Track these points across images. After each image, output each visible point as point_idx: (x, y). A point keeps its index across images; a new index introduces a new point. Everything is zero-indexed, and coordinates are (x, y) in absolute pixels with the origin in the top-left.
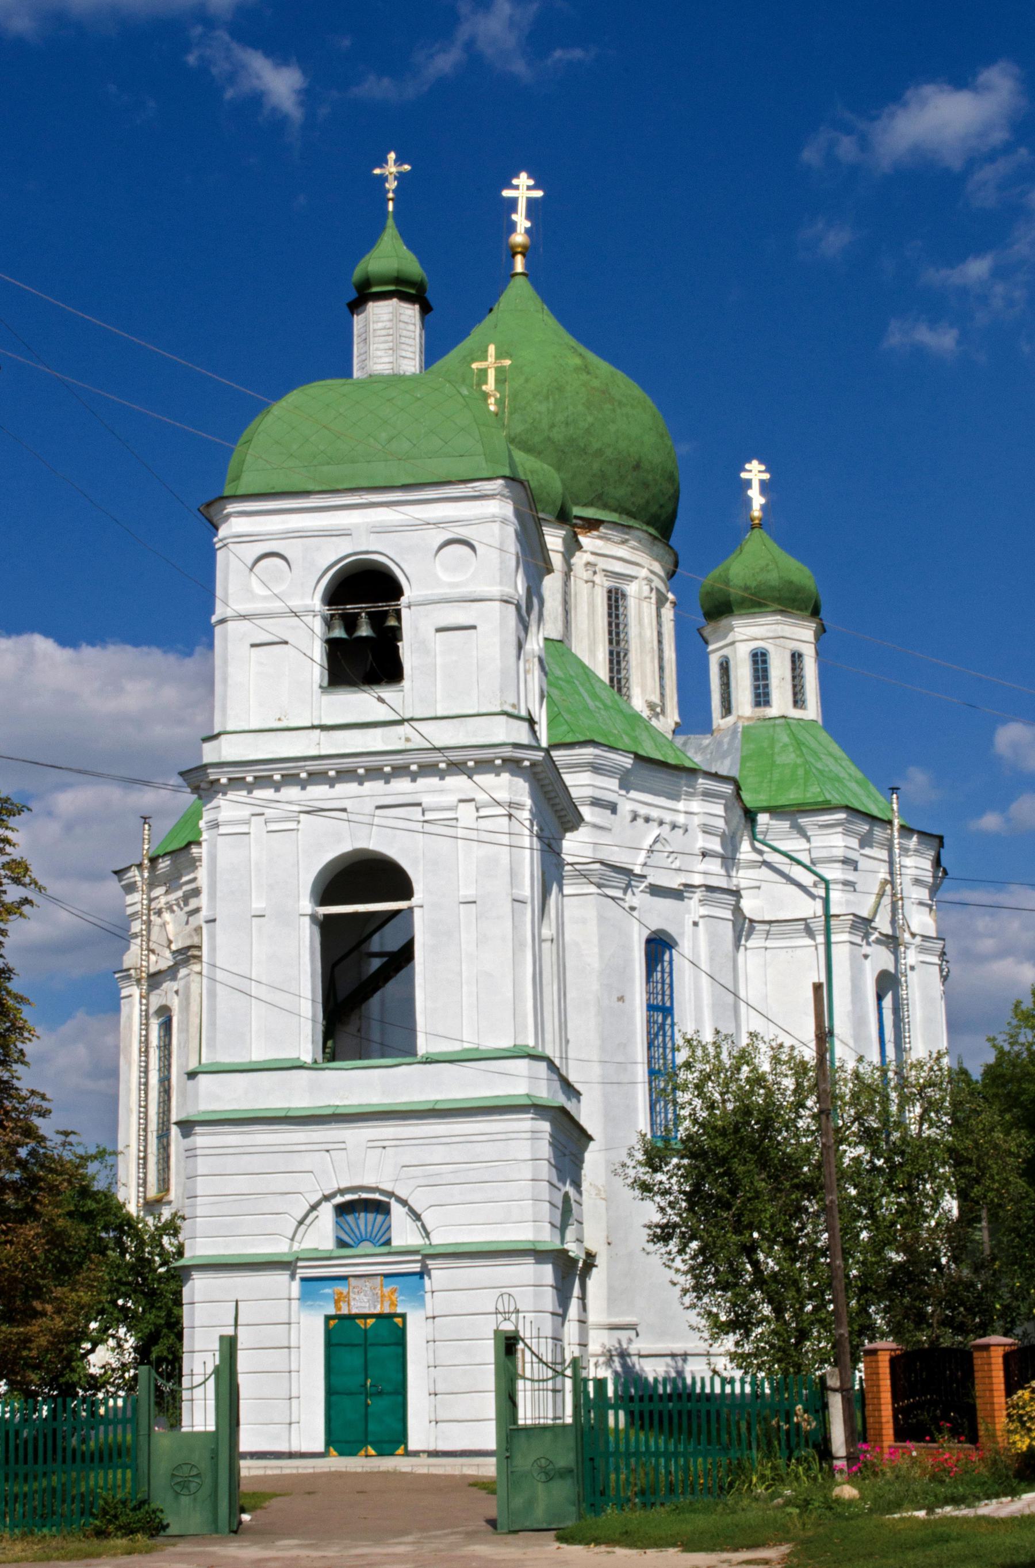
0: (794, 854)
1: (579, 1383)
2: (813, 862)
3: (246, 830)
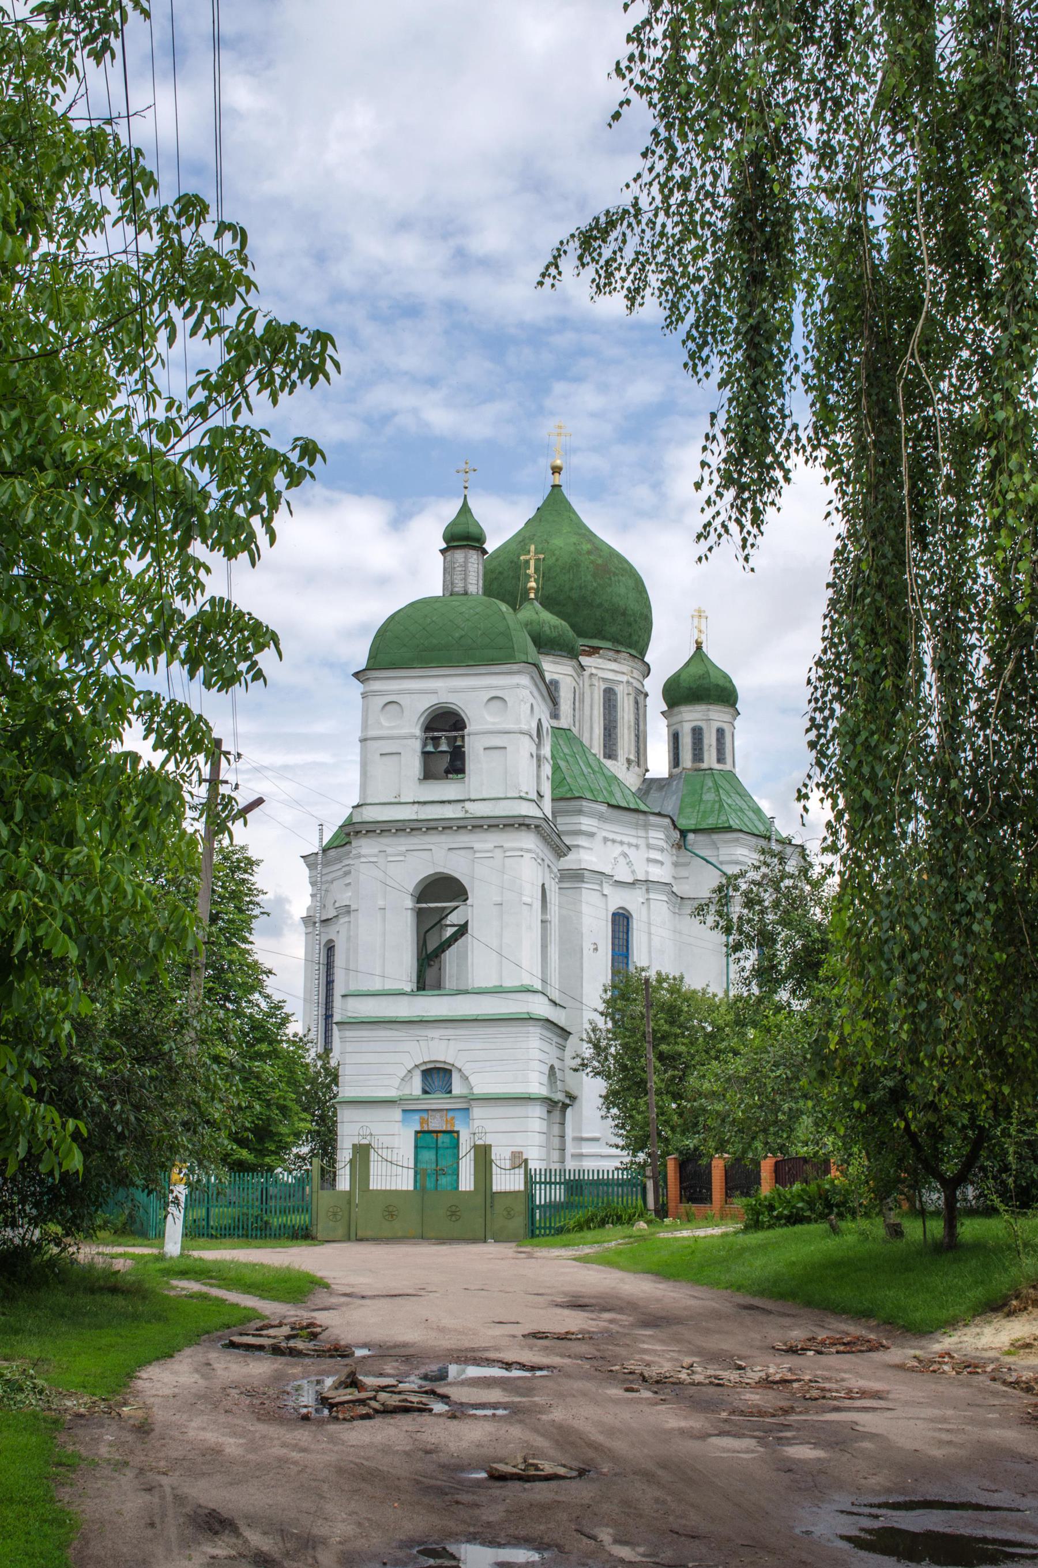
2: (721, 863)
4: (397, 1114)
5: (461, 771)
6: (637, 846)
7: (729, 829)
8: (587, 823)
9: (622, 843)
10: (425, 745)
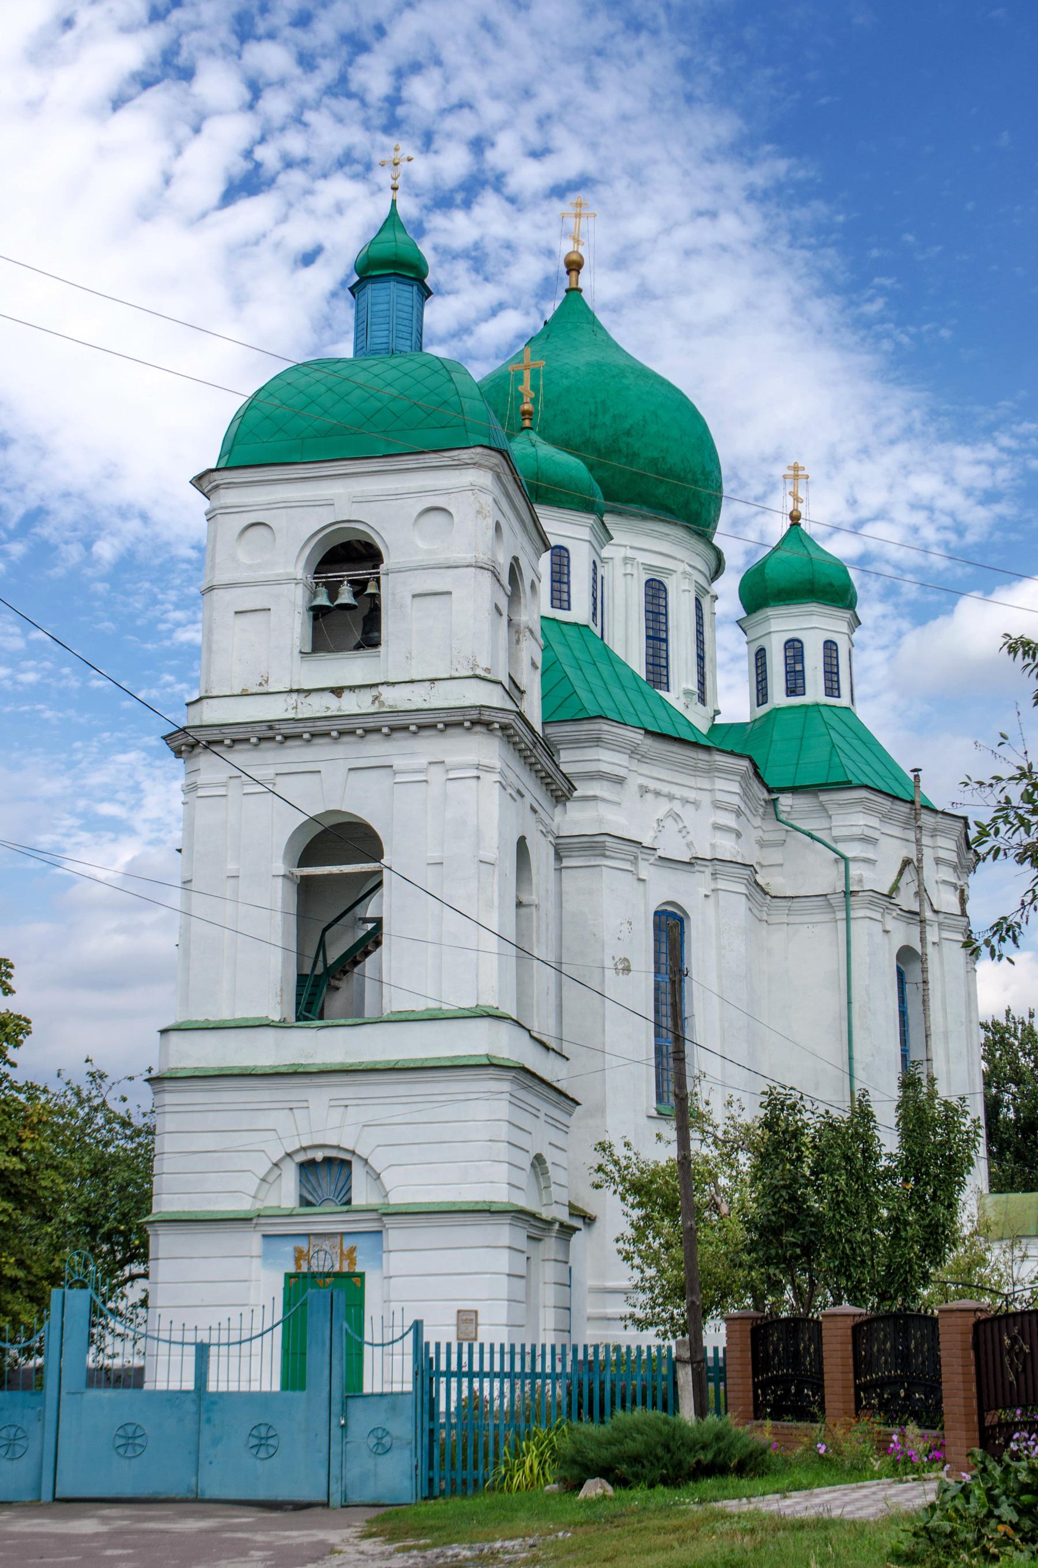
0: (814, 833)
1: (420, 1348)
2: (836, 840)
3: (224, 793)
4: (253, 1242)
5: (375, 644)
6: (696, 804)
7: (846, 785)
8: (608, 760)
9: (671, 797)
10: (314, 595)
